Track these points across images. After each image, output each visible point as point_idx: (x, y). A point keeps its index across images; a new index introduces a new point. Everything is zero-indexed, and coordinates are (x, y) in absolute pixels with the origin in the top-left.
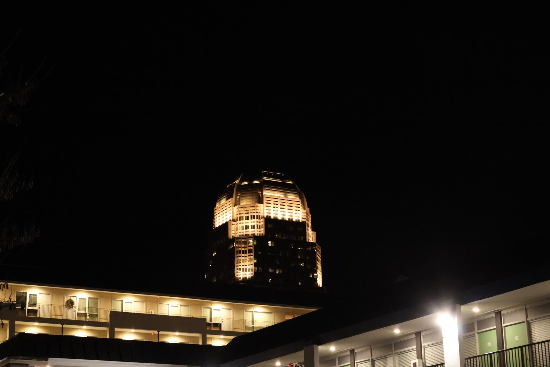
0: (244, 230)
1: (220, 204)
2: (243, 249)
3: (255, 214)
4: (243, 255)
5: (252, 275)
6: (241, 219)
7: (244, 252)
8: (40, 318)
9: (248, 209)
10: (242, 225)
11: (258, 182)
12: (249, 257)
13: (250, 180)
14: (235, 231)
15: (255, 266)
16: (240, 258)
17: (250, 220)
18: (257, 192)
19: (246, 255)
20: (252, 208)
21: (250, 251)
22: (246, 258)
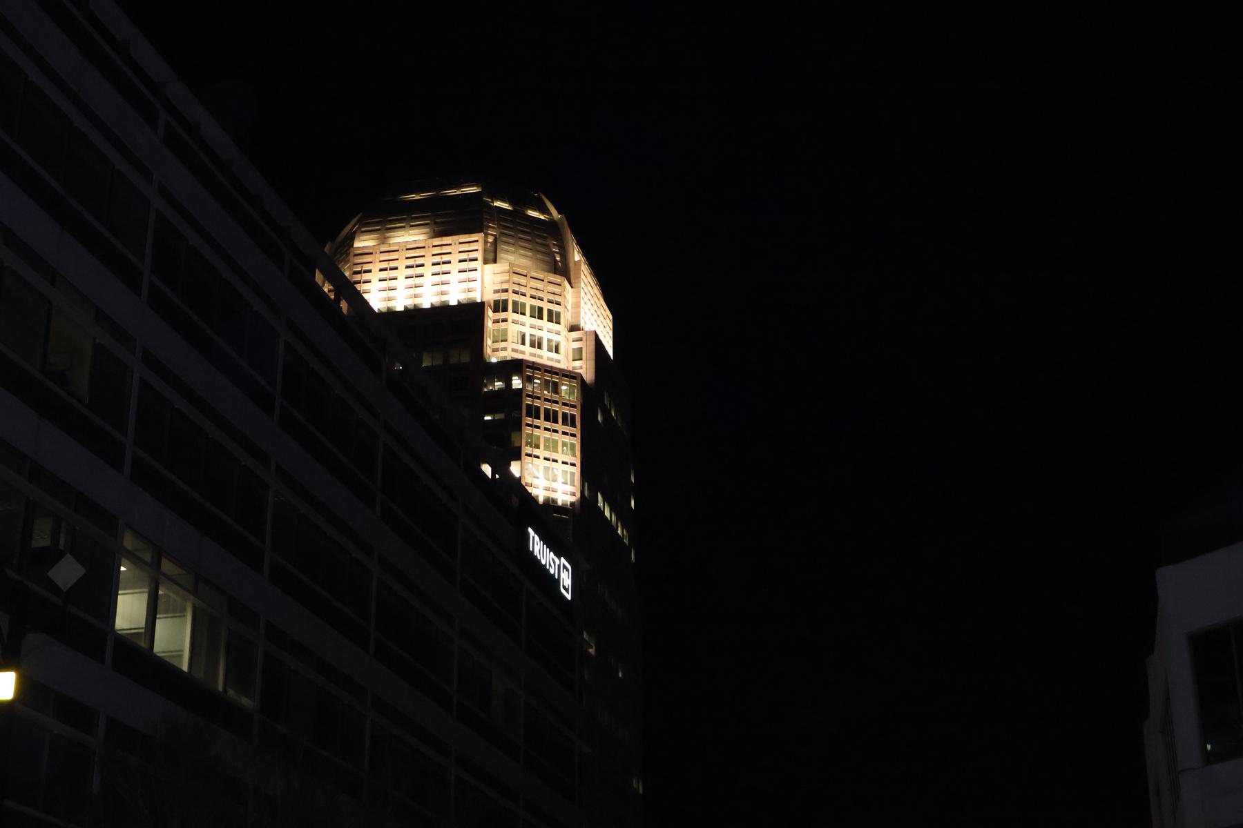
0: (527, 348)
1: (384, 241)
2: (548, 406)
3: (546, 306)
4: (548, 425)
5: (573, 499)
6: (518, 309)
7: (551, 417)
8: (51, 581)
9: (523, 280)
10: (523, 329)
11: (505, 206)
12: (567, 439)
13: (521, 202)
14: (506, 339)
15: (520, 448)
16: (537, 432)
17: (544, 323)
18: (547, 246)
19: (555, 427)
20: (534, 284)
21: (568, 420)
22: (555, 436)
